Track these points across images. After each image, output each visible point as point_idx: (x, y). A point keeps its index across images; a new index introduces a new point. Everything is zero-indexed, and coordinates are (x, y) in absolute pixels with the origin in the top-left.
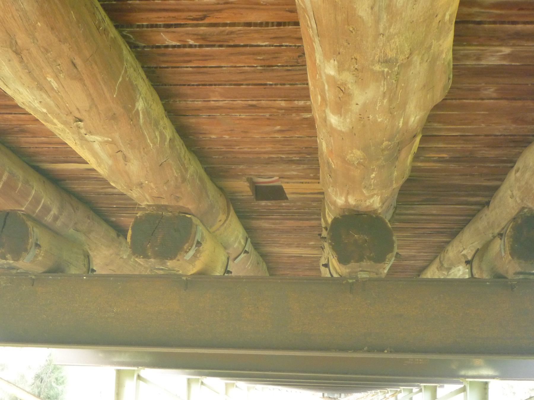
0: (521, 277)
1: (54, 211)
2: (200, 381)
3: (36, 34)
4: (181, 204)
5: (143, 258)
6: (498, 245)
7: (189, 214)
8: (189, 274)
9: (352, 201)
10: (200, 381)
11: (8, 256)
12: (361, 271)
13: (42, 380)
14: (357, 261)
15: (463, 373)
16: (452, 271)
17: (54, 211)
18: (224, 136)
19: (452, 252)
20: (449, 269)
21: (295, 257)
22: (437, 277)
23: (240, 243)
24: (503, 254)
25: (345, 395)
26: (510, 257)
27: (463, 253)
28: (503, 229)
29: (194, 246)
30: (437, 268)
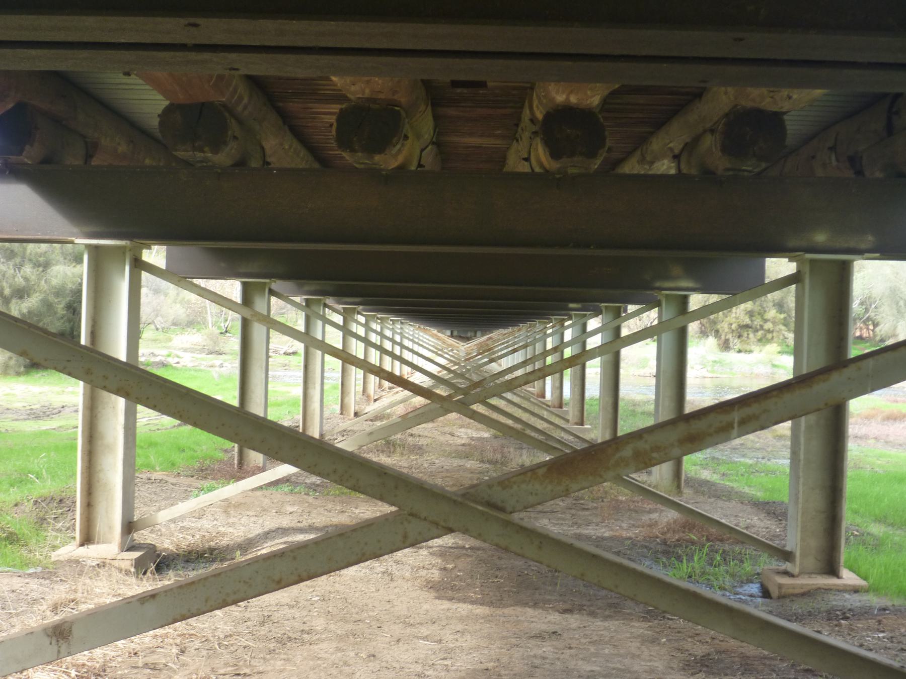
0: (731, 173)
1: (245, 100)
3: (550, 87)
4: (396, 97)
6: (708, 141)
7: (398, 107)
8: (390, 168)
9: (573, 99)
10: (322, 302)
11: (206, 149)
12: (571, 166)
13: (74, 312)
15: (658, 284)
16: (656, 165)
17: (245, 100)
19: (656, 144)
20: (652, 163)
21: (473, 147)
22: (636, 172)
24: (714, 150)
25: (482, 334)
26: (720, 154)
27: (669, 146)
28: (715, 123)
29: (401, 140)
30: (638, 162)
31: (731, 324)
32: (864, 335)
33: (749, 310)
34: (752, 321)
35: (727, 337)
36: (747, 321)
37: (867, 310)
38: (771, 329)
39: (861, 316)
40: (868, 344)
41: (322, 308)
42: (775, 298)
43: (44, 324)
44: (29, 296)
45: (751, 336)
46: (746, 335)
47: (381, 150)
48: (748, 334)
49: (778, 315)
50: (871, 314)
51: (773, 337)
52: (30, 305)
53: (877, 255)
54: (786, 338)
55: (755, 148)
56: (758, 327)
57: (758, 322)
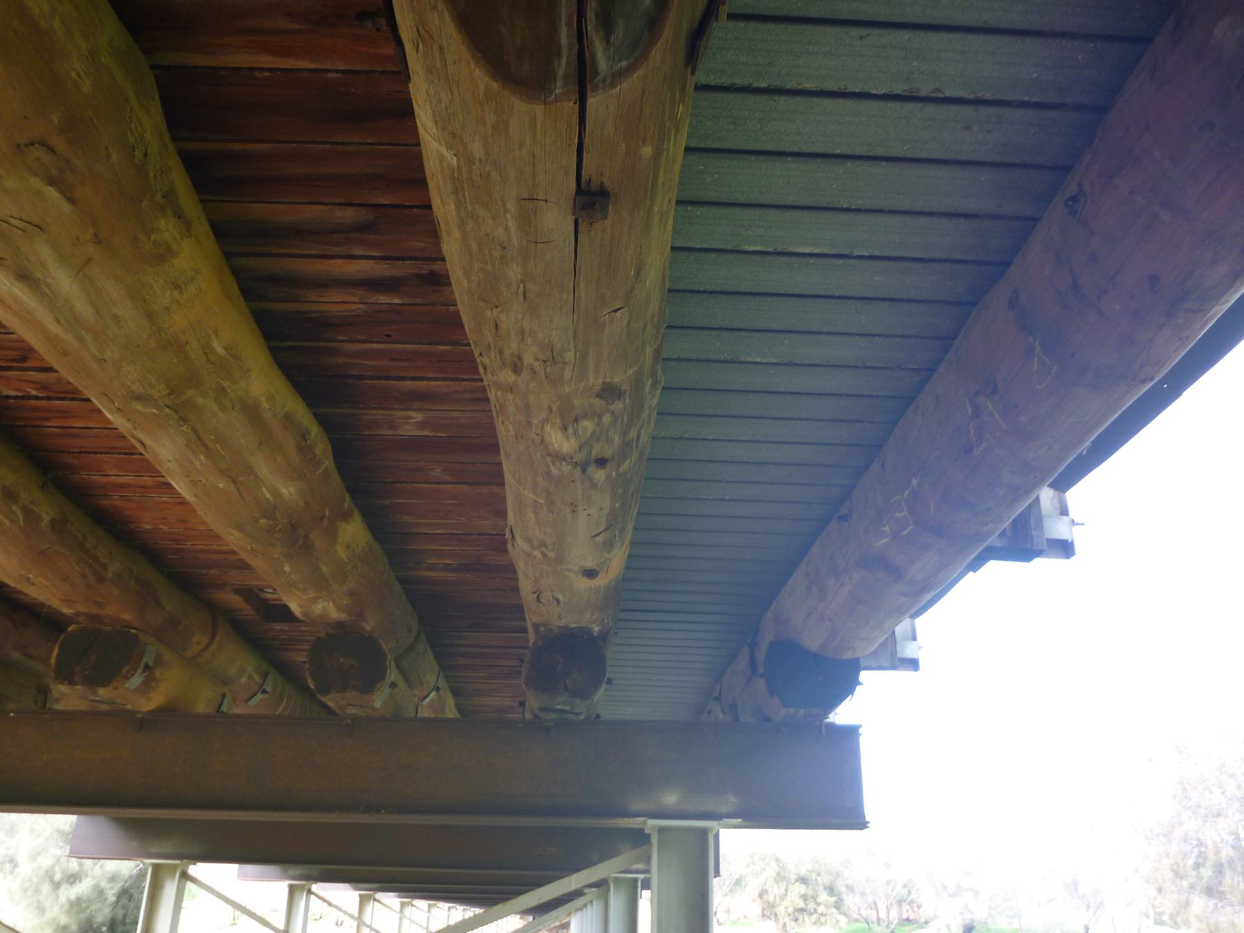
2: (307, 888)
5: (68, 684)
10: (307, 888)
14: (338, 692)
18: (161, 527)
23: (250, 677)
29: (140, 671)
31: (787, 908)
32: (911, 918)
33: (802, 893)
34: (806, 904)
35: (785, 921)
36: (801, 905)
37: (910, 892)
38: (824, 913)
39: (905, 898)
40: (915, 926)
41: (305, 894)
42: (825, 881)
43: (92, 910)
44: (80, 881)
45: (806, 919)
46: (802, 918)
47: (105, 683)
48: (803, 918)
49: (829, 898)
50: (913, 896)
51: (826, 921)
52: (80, 891)
53: (739, 820)
54: (838, 921)
55: (567, 682)
56: (812, 910)
57: (811, 906)
